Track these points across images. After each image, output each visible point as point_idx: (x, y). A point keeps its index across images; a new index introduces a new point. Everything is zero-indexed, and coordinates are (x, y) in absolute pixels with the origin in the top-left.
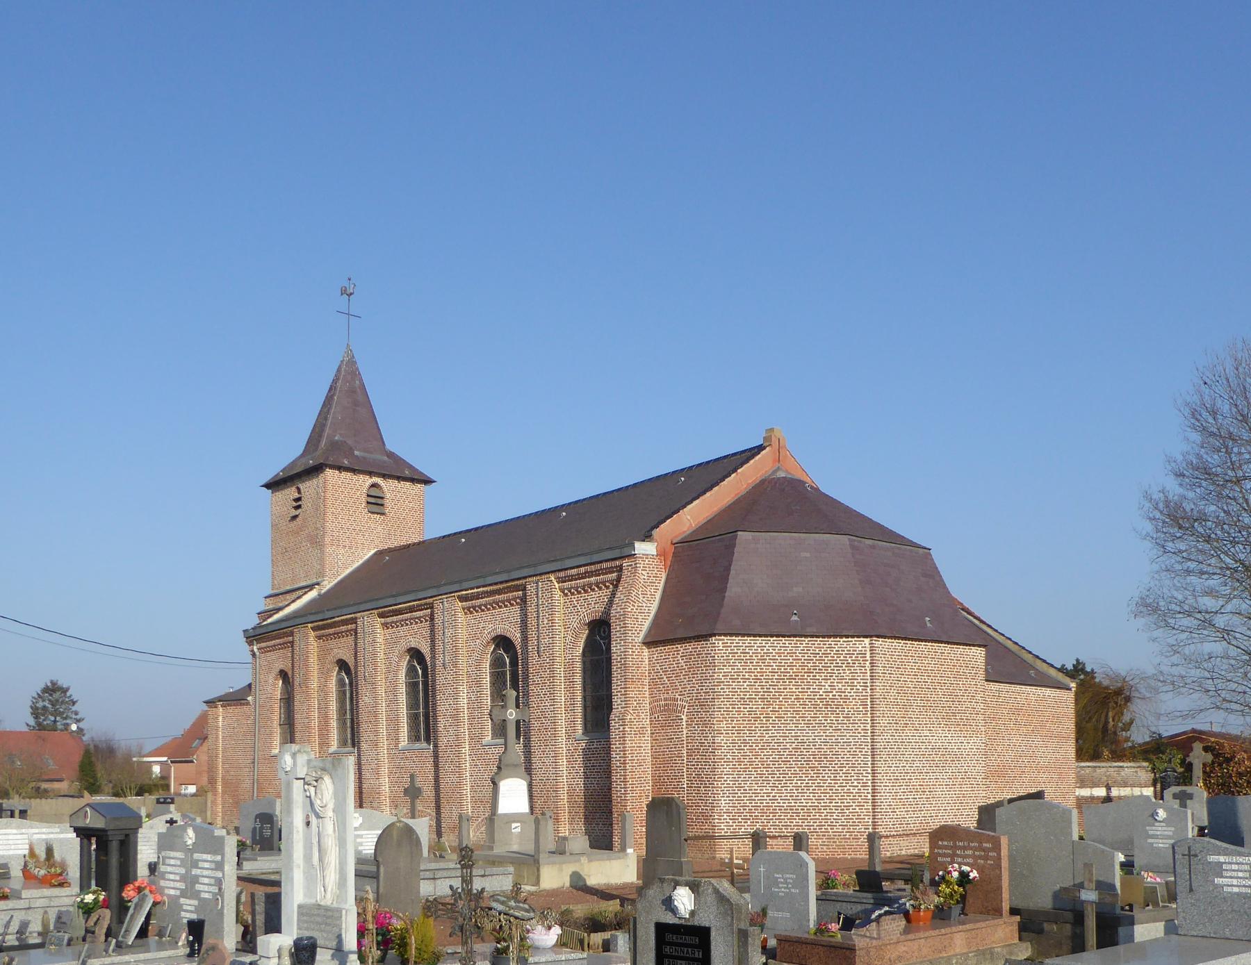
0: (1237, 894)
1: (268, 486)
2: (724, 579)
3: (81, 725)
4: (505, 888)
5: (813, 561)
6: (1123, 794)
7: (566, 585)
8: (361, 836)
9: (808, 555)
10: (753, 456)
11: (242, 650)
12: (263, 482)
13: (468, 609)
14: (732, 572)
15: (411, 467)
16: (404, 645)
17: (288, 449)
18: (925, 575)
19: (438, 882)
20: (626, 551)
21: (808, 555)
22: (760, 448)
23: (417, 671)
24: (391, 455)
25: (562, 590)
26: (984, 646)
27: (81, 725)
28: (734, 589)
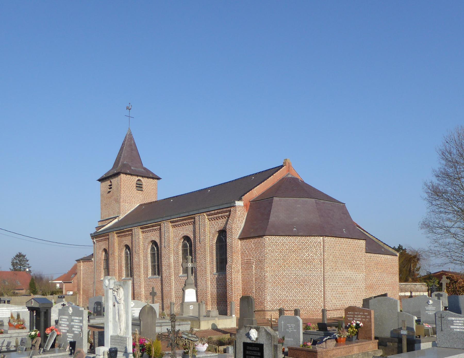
0: (459, 332)
1: (99, 180)
2: (269, 215)
3: (30, 269)
4: (187, 330)
5: (302, 208)
6: (416, 294)
7: (210, 217)
8: (134, 310)
9: (300, 206)
10: (279, 169)
11: (90, 241)
12: (98, 179)
13: (174, 226)
14: (272, 212)
15: (152, 173)
16: (150, 239)
17: (107, 167)
18: (343, 213)
19: (163, 327)
20: (232, 205)
21: (300, 206)
22: (282, 166)
23: (155, 249)
24: (145, 169)
25: (209, 219)
26: (365, 240)
27: (30, 269)
28: (272, 218)
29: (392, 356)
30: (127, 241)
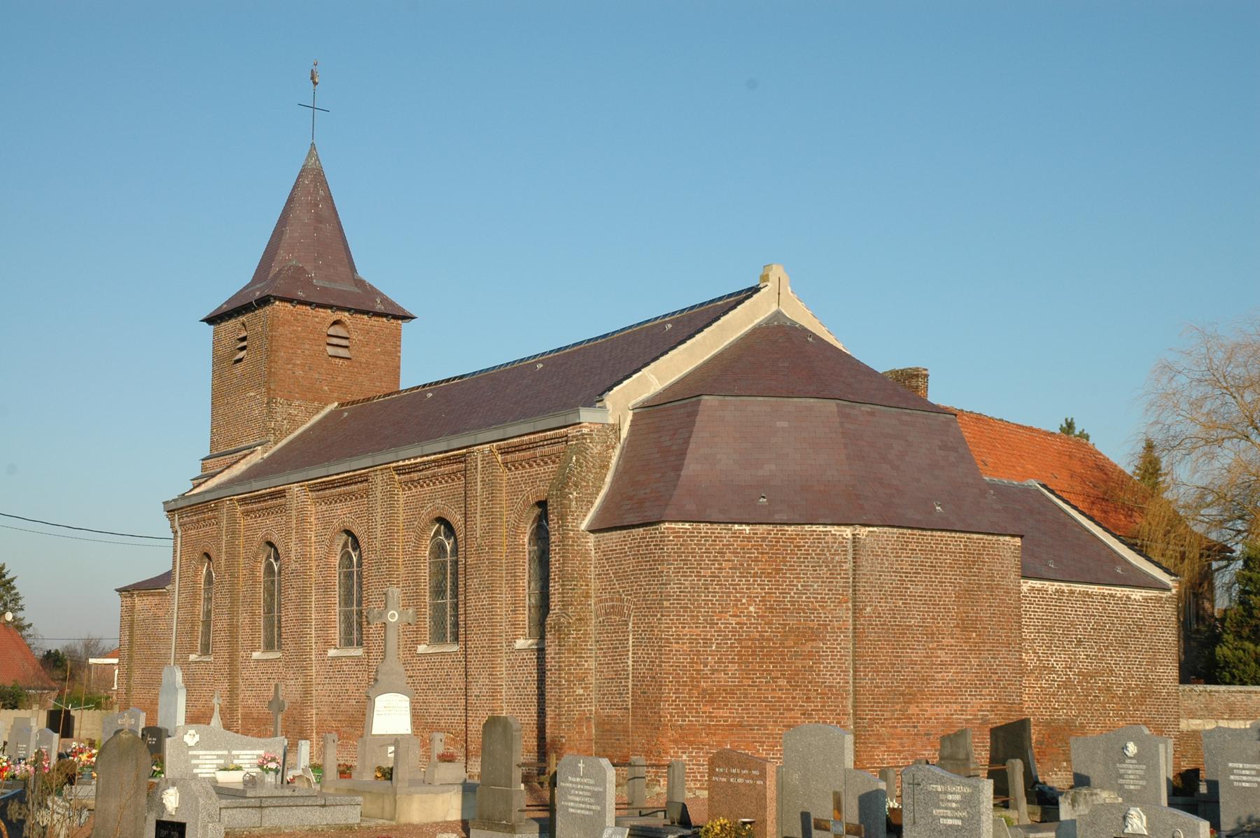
0: (951, 826)
1: (212, 320)
2: (682, 454)
3: (20, 614)
4: (351, 821)
5: (795, 432)
6: (1198, 721)
7: (509, 457)
8: (197, 757)
9: (785, 424)
10: (750, 296)
11: (163, 526)
12: (205, 316)
13: (406, 483)
14: (692, 446)
15: (385, 300)
16: (428, 511)
17: (235, 278)
18: (944, 447)
19: (266, 811)
20: (571, 419)
21: (785, 424)
22: (755, 290)
23: (351, 558)
24: (361, 283)
25: (505, 464)
26: (1021, 537)
27: (20, 614)
28: (691, 467)
29: (445, 835)
30: (268, 526)
